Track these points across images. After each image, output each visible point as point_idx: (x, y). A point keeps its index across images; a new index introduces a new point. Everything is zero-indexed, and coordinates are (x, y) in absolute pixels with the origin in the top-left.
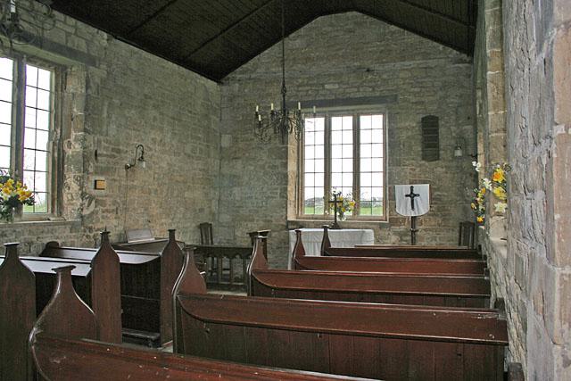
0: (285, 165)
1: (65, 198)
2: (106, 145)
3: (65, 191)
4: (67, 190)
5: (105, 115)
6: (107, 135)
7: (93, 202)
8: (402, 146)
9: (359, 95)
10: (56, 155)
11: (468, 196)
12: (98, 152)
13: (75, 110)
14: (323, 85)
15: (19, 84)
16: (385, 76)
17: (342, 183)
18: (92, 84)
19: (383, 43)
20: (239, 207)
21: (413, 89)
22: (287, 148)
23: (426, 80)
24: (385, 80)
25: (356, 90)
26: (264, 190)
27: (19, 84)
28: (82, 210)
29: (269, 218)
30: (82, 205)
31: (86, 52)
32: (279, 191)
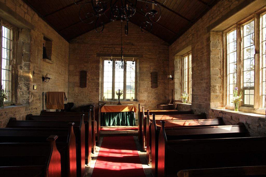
0: (99, 80)
1: (19, 94)
2: (37, 68)
3: (19, 90)
4: (19, 90)
5: (36, 54)
6: (37, 64)
7: (33, 96)
8: (144, 74)
9: (129, 53)
10: (13, 72)
11: (167, 92)
12: (35, 72)
13: (24, 51)
14: (114, 48)
15: (190, 51)
16: (138, 47)
17: (119, 86)
18: (33, 39)
19: (138, 35)
20: (77, 96)
21: (148, 53)
22: (99, 72)
23: (153, 50)
24: (138, 48)
25: (128, 51)
26: (89, 88)
27: (190, 51)
28: (29, 99)
29: (91, 100)
30: (29, 97)
31: (31, 22)
32: (95, 89)
